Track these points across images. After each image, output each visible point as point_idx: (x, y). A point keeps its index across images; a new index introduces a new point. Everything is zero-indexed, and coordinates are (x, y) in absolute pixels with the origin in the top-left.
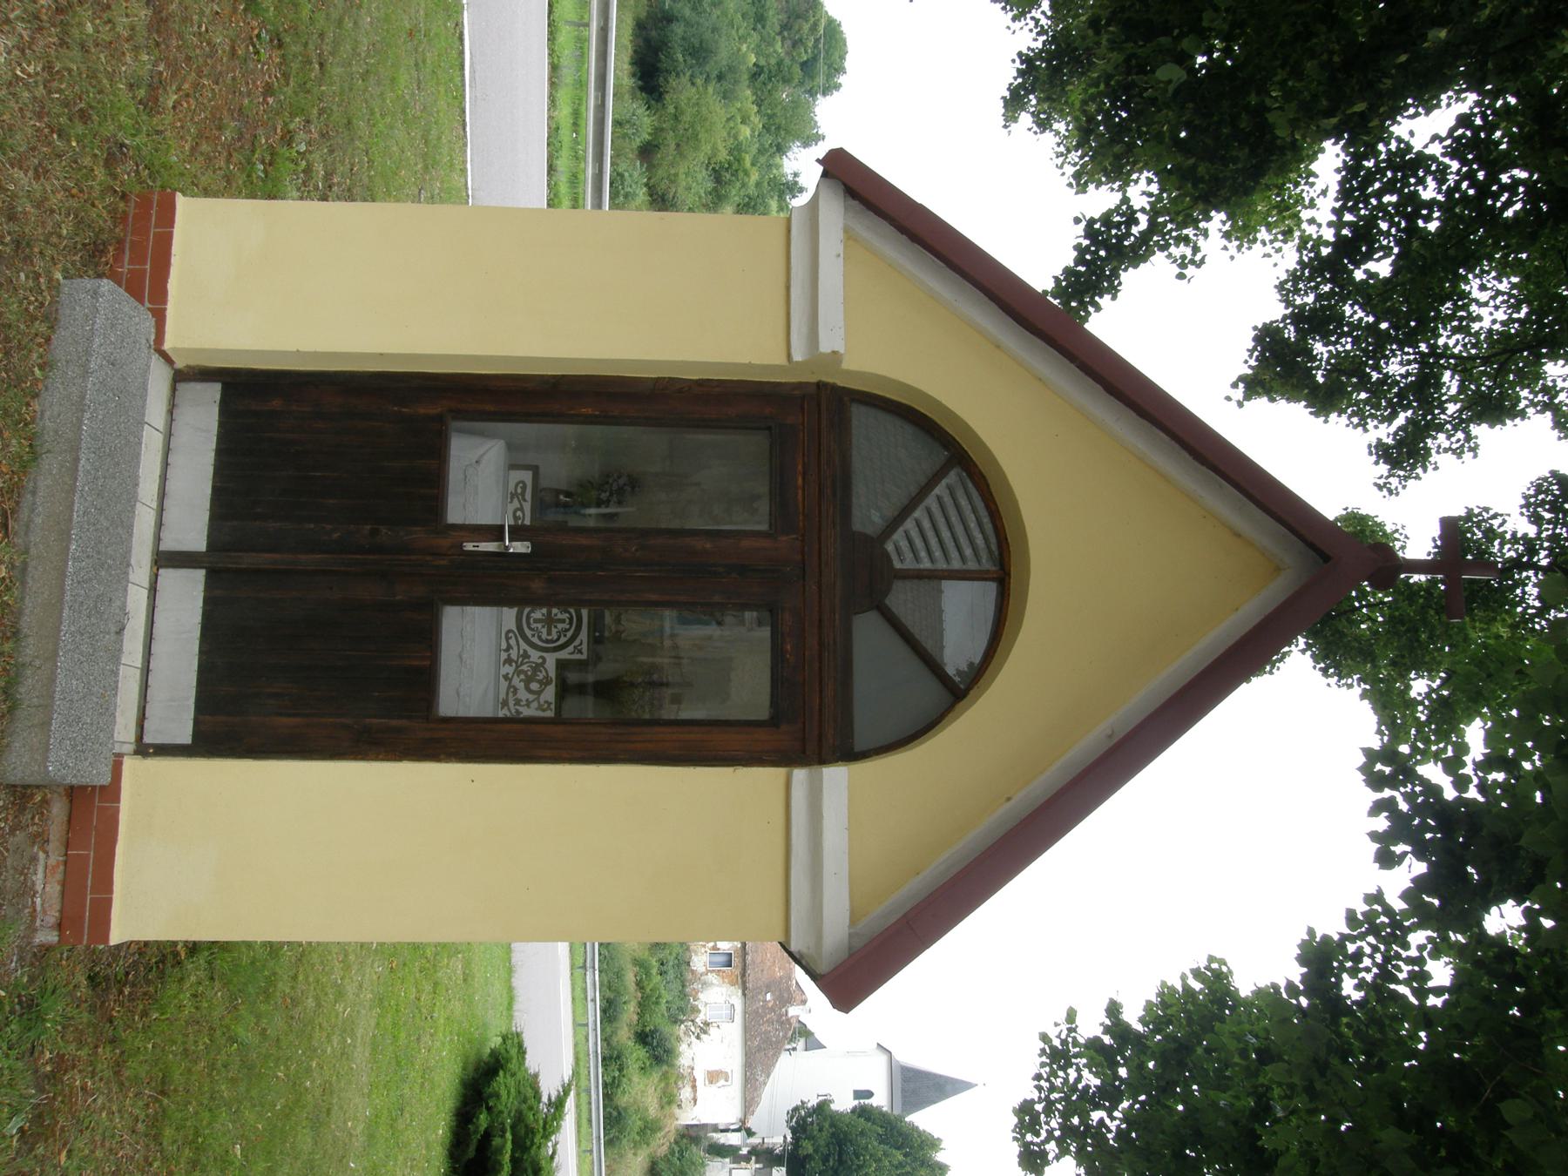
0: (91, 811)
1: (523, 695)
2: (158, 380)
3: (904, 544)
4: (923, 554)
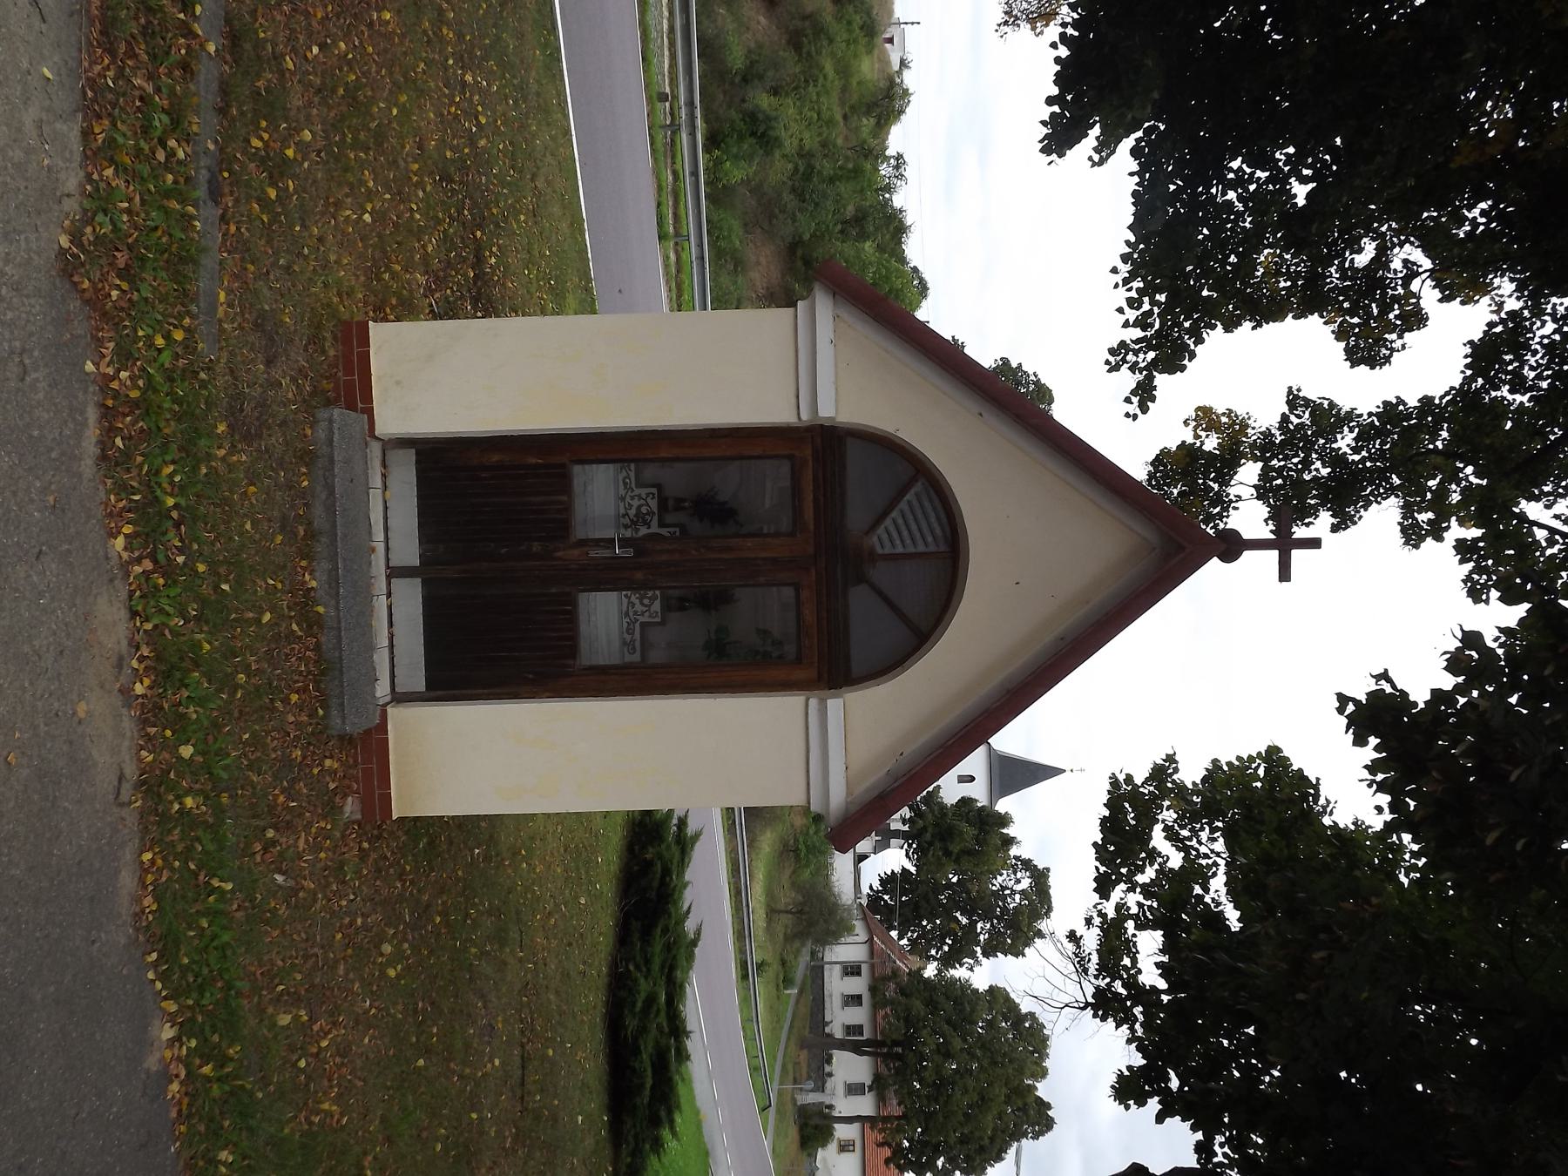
0: (370, 749)
1: (639, 608)
2: (375, 449)
3: (885, 537)
4: (898, 542)
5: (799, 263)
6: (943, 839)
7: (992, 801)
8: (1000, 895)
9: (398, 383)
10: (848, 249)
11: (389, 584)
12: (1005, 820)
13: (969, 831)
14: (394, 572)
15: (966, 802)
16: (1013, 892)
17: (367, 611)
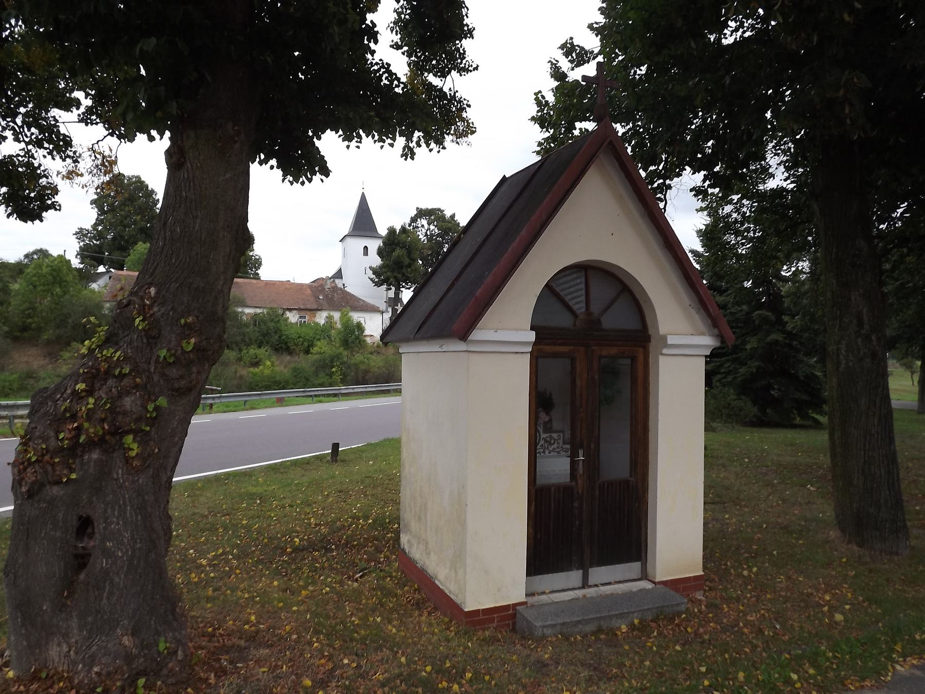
1: (555, 446)
5: (26, 334)
6: (402, 267)
7: (380, 237)
8: (430, 238)
9: (499, 590)
10: (14, 302)
11: (590, 586)
12: (392, 231)
13: (398, 252)
14: (585, 584)
15: (380, 253)
16: (428, 229)
17: (612, 597)
